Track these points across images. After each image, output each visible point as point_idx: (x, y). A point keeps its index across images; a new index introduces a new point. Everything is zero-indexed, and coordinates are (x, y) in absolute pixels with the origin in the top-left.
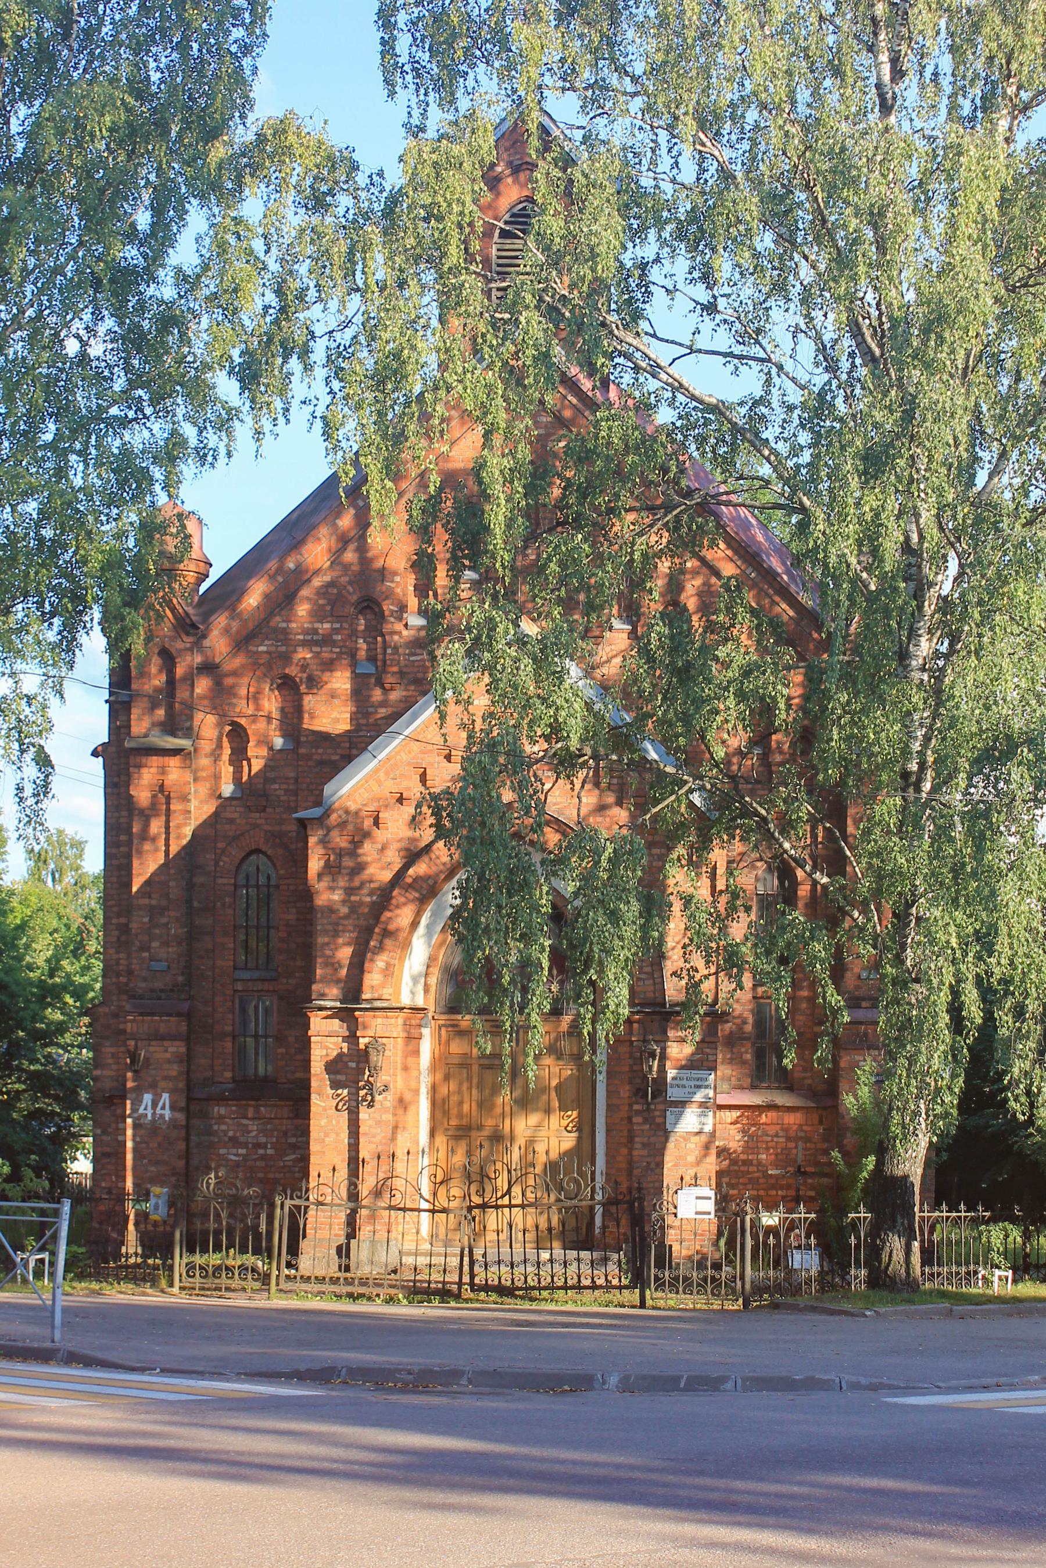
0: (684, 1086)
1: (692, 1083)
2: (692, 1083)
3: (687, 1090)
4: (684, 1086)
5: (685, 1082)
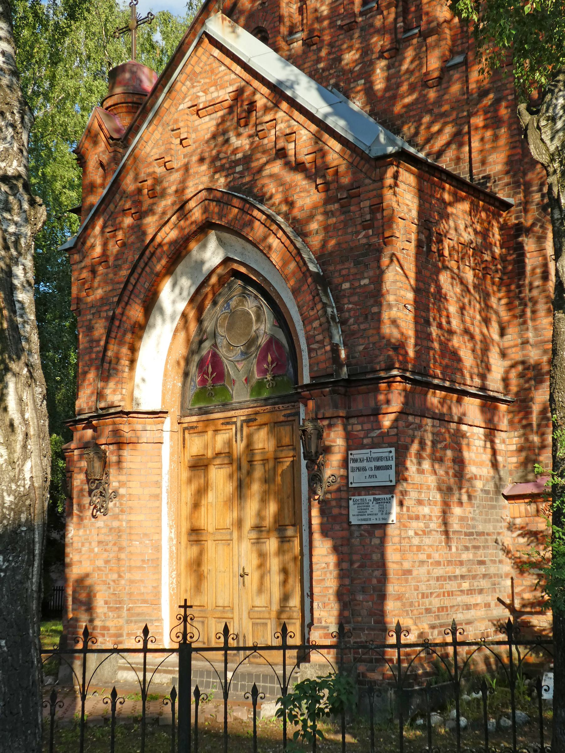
0: (364, 469)
1: (373, 464)
2: (373, 464)
3: (368, 473)
4: (364, 469)
5: (365, 464)
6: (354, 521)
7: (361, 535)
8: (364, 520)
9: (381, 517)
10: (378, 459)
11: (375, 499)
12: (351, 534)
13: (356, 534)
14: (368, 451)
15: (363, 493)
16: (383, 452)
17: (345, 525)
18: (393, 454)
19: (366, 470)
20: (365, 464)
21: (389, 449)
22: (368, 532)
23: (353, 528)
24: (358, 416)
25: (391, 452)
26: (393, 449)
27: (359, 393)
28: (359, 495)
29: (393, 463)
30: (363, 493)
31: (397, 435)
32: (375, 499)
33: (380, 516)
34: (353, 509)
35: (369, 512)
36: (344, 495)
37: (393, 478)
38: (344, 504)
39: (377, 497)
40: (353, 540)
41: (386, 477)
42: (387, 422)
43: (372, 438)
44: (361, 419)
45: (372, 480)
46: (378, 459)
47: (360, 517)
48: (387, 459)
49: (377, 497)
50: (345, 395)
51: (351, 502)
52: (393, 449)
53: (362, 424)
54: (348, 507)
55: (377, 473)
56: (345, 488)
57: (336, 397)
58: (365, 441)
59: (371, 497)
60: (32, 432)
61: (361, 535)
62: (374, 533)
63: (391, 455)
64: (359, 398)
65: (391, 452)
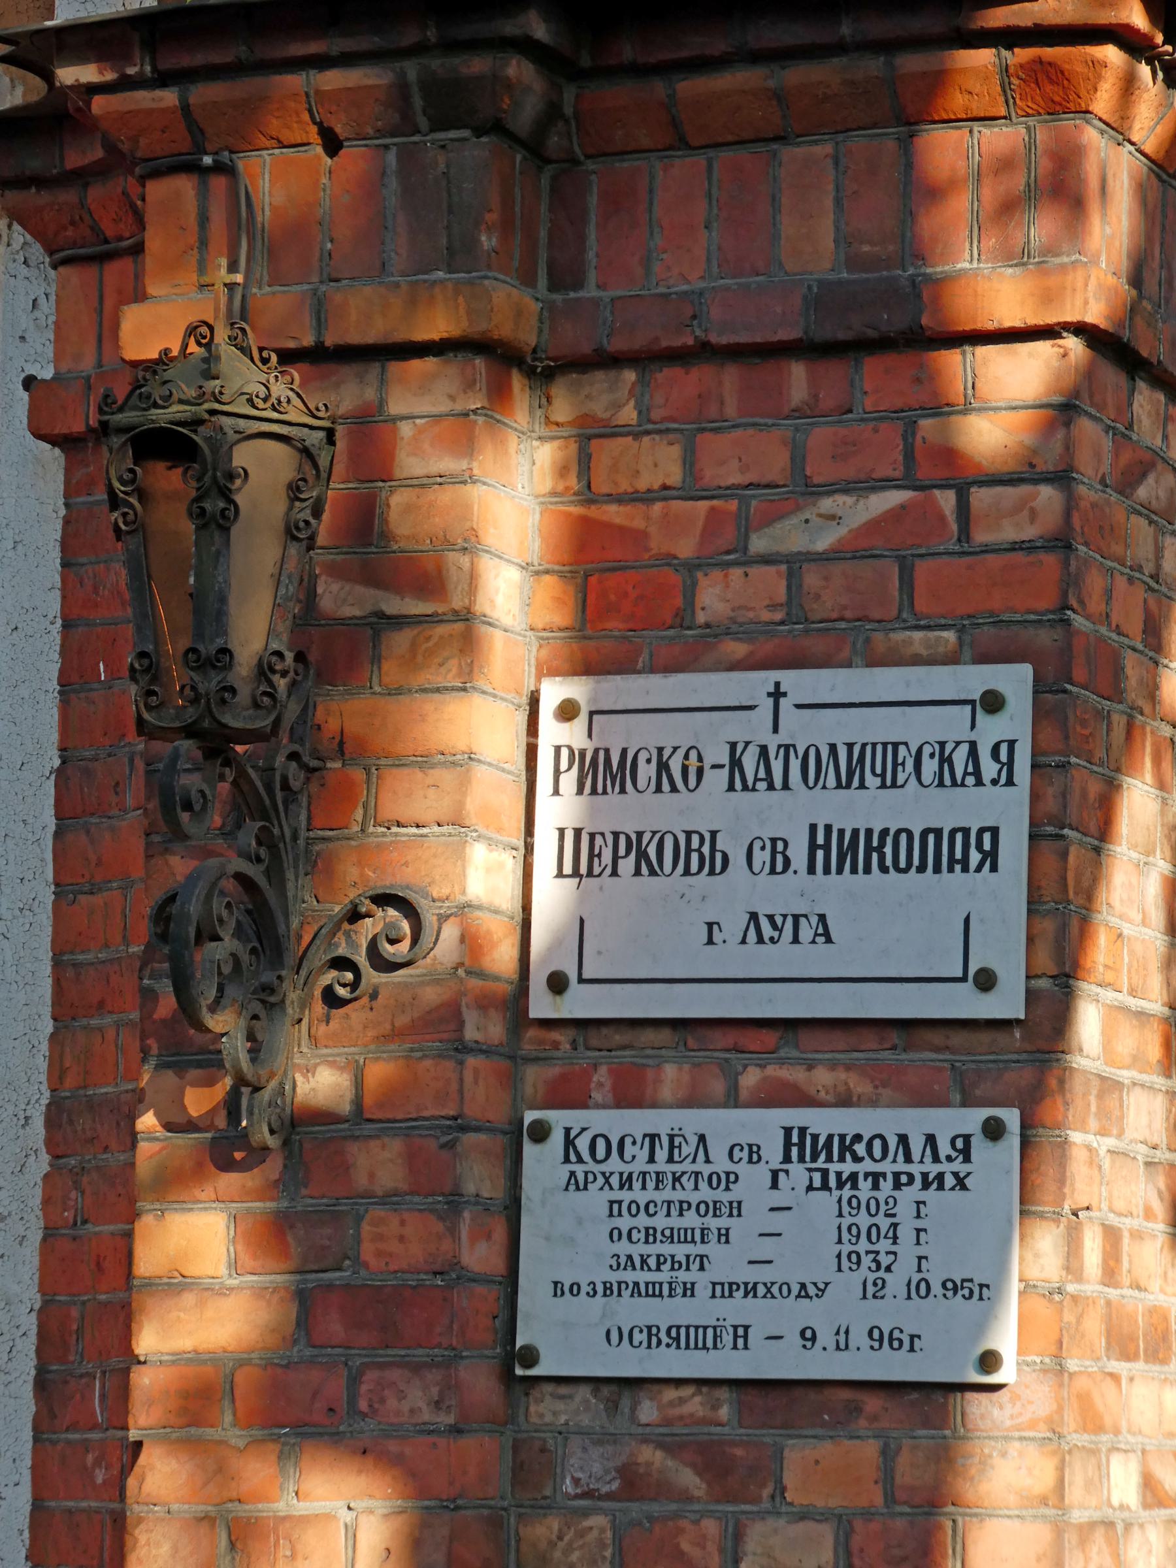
0: (703, 855)
1: (792, 813)
2: (792, 813)
3: (741, 891)
4: (703, 855)
5: (709, 807)
6: (565, 1337)
7: (633, 1483)
8: (679, 1337)
9: (862, 1317)
10: (853, 767)
11: (796, 1143)
12: (531, 1466)
13: (585, 1467)
14: (754, 685)
15: (672, 1076)
16: (920, 699)
17: (479, 1380)
18: (1015, 723)
19: (715, 863)
20: (709, 807)
21: (975, 679)
22: (712, 1460)
23: (546, 1410)
24: (645, 360)
25: (993, 702)
26: (1015, 681)
27: (679, 142)
28: (629, 1096)
29: (1008, 809)
30: (672, 1076)
31: (1060, 542)
32: (796, 1143)
33: (844, 1304)
34: (566, 1231)
35: (726, 1263)
36: (481, 1093)
37: (1005, 949)
38: (479, 1178)
39: (825, 1122)
40: (544, 1529)
41: (906, 943)
42: (1004, 395)
43: (794, 564)
44: (679, 386)
45: (779, 958)
46: (853, 767)
47: (634, 1312)
48: (951, 769)
49: (825, 1122)
50: (534, 148)
51: (541, 1165)
52: (1015, 681)
53: (693, 428)
54: (513, 1208)
55: (835, 893)
56: (495, 1030)
57: (468, 156)
58: (713, 598)
59: (766, 1126)
60: (1052, 1209)
61: (633, 1483)
62: (768, 1468)
63: (992, 729)
64: (674, 181)
65: (993, 702)
